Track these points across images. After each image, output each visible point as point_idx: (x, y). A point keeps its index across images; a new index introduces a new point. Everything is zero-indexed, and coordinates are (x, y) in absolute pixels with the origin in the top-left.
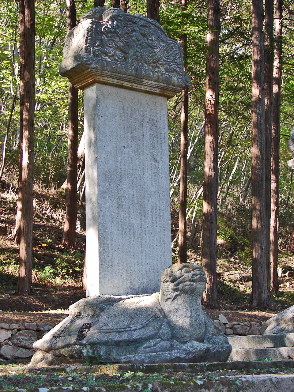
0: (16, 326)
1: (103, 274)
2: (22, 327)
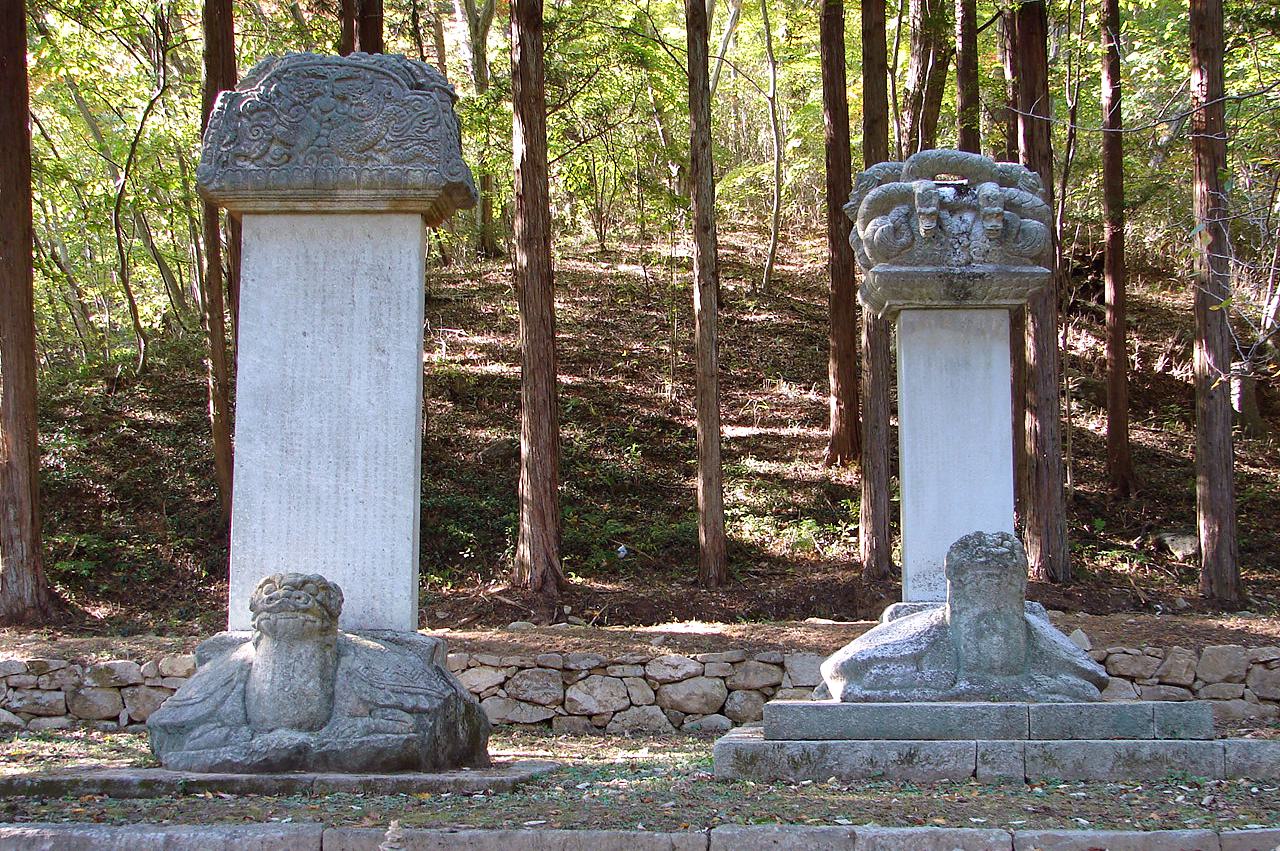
0: (515, 660)
2: (528, 663)
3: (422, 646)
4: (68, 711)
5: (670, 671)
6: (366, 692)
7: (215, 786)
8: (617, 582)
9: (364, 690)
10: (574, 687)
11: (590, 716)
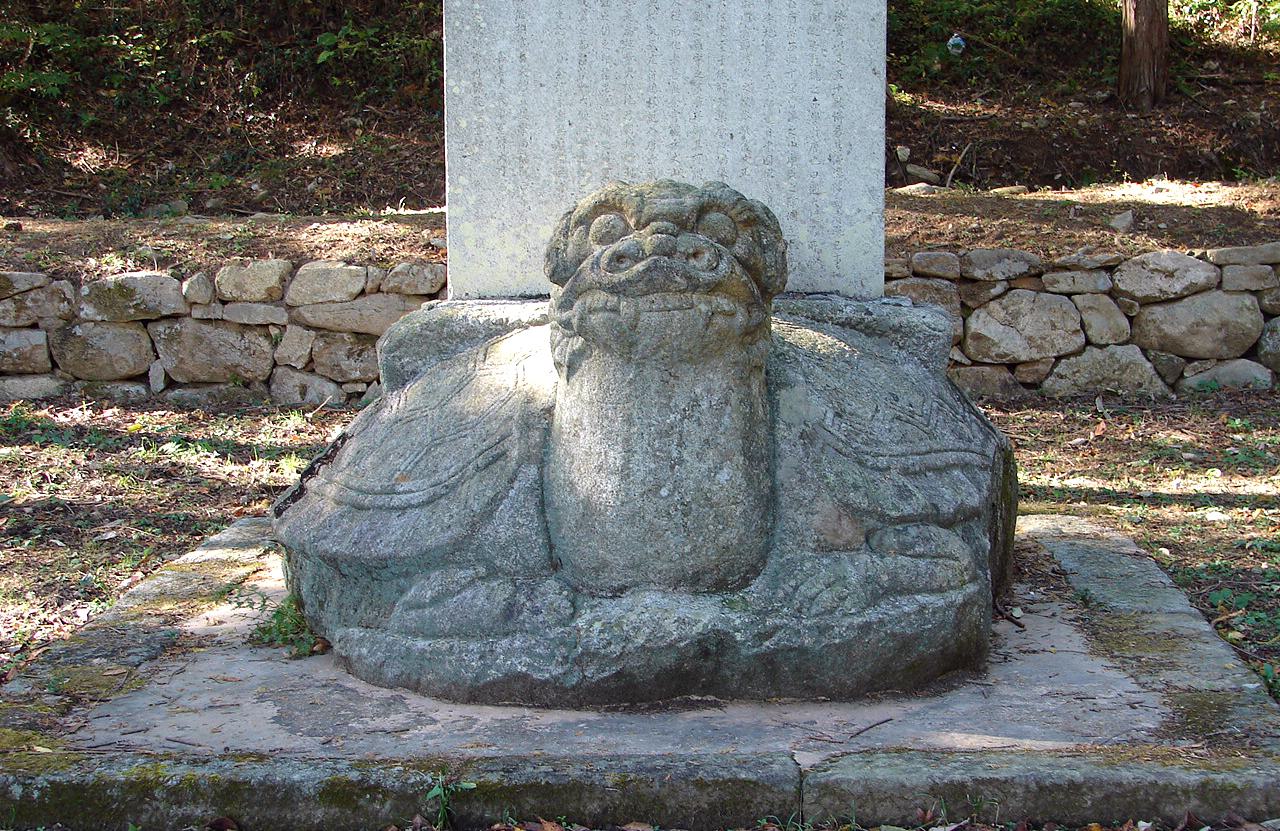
1: (472, 200)
3: (929, 337)
4: (55, 365)
5: (1161, 282)
6: (856, 487)
7: (530, 802)
8: (968, 99)
9: (850, 479)
10: (983, 314)
11: (1012, 366)
